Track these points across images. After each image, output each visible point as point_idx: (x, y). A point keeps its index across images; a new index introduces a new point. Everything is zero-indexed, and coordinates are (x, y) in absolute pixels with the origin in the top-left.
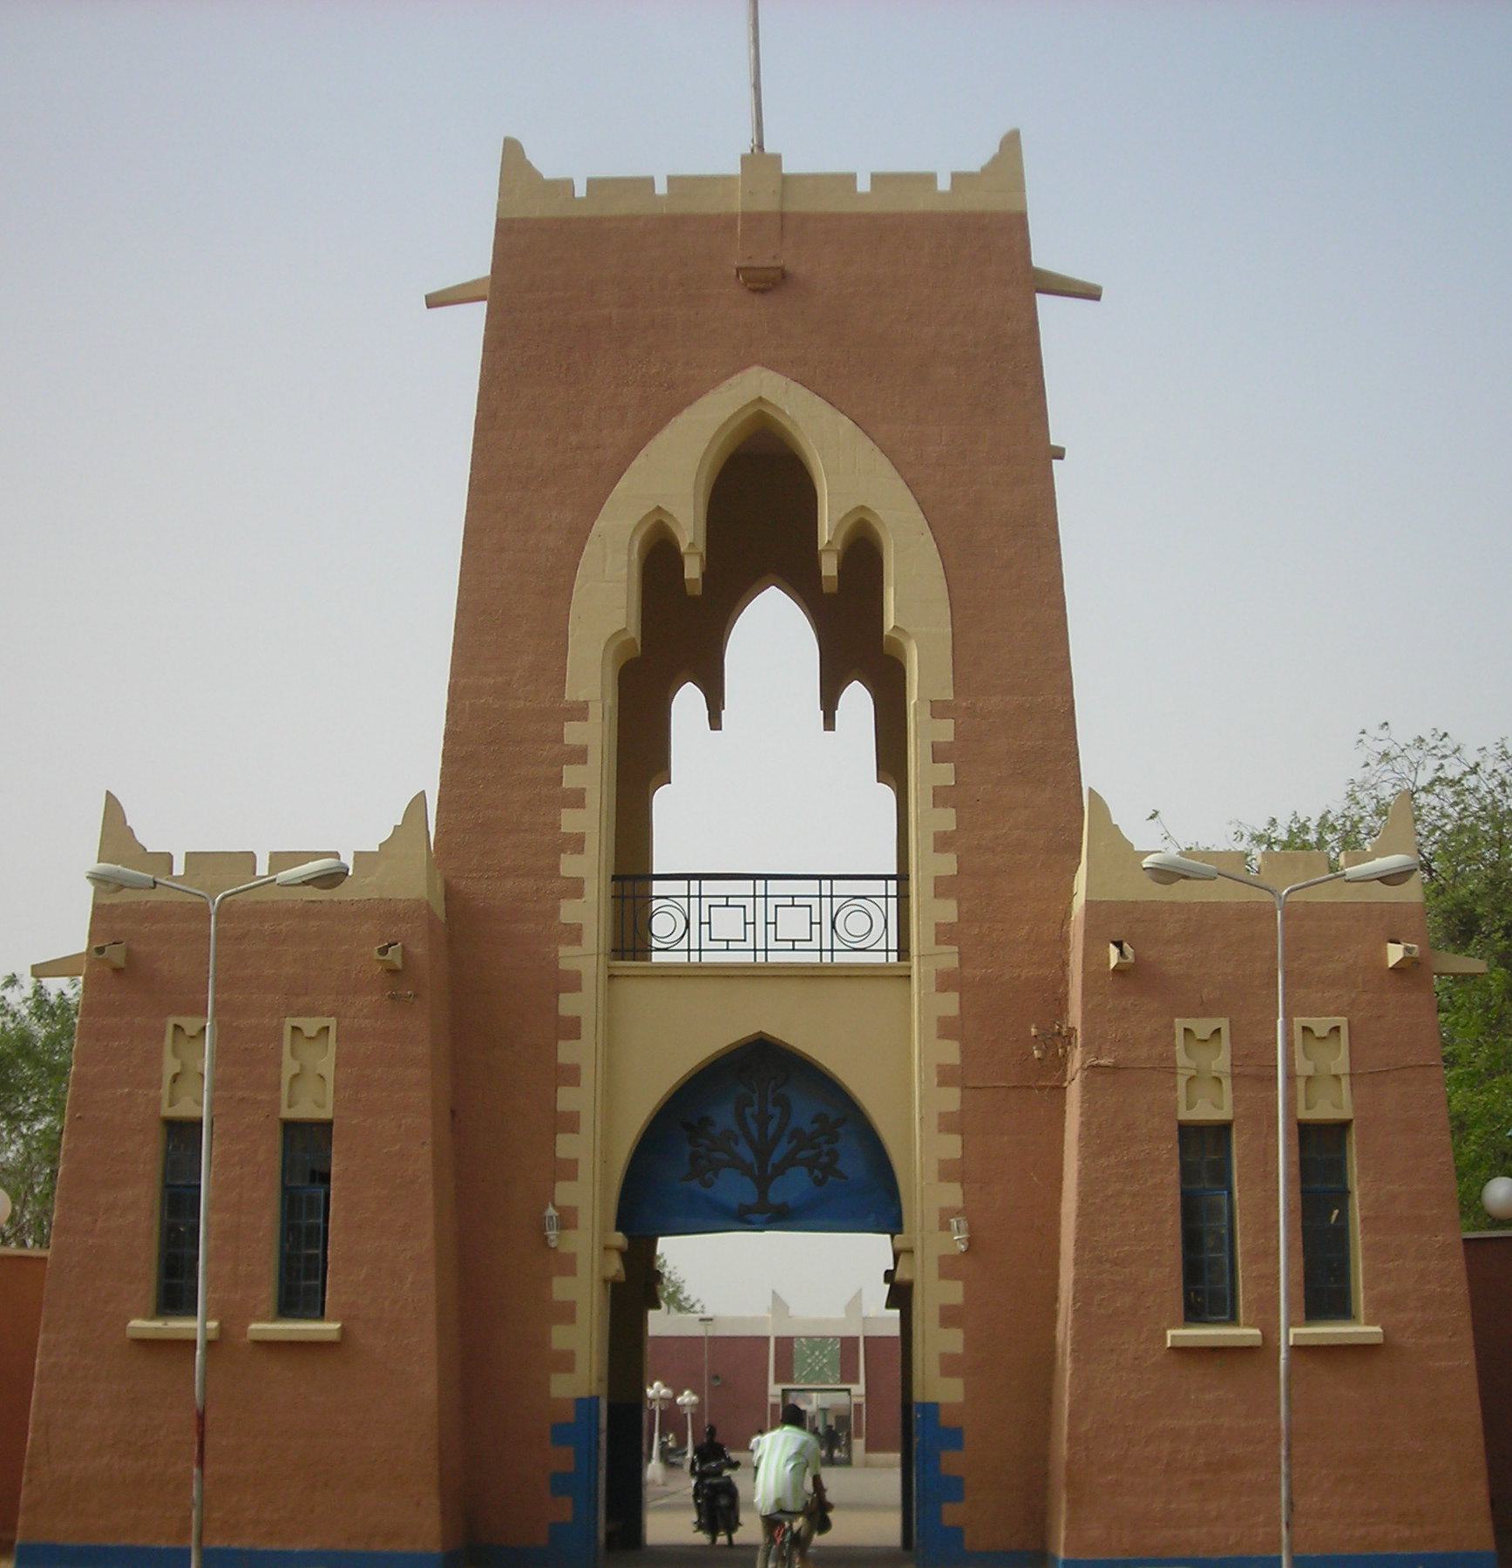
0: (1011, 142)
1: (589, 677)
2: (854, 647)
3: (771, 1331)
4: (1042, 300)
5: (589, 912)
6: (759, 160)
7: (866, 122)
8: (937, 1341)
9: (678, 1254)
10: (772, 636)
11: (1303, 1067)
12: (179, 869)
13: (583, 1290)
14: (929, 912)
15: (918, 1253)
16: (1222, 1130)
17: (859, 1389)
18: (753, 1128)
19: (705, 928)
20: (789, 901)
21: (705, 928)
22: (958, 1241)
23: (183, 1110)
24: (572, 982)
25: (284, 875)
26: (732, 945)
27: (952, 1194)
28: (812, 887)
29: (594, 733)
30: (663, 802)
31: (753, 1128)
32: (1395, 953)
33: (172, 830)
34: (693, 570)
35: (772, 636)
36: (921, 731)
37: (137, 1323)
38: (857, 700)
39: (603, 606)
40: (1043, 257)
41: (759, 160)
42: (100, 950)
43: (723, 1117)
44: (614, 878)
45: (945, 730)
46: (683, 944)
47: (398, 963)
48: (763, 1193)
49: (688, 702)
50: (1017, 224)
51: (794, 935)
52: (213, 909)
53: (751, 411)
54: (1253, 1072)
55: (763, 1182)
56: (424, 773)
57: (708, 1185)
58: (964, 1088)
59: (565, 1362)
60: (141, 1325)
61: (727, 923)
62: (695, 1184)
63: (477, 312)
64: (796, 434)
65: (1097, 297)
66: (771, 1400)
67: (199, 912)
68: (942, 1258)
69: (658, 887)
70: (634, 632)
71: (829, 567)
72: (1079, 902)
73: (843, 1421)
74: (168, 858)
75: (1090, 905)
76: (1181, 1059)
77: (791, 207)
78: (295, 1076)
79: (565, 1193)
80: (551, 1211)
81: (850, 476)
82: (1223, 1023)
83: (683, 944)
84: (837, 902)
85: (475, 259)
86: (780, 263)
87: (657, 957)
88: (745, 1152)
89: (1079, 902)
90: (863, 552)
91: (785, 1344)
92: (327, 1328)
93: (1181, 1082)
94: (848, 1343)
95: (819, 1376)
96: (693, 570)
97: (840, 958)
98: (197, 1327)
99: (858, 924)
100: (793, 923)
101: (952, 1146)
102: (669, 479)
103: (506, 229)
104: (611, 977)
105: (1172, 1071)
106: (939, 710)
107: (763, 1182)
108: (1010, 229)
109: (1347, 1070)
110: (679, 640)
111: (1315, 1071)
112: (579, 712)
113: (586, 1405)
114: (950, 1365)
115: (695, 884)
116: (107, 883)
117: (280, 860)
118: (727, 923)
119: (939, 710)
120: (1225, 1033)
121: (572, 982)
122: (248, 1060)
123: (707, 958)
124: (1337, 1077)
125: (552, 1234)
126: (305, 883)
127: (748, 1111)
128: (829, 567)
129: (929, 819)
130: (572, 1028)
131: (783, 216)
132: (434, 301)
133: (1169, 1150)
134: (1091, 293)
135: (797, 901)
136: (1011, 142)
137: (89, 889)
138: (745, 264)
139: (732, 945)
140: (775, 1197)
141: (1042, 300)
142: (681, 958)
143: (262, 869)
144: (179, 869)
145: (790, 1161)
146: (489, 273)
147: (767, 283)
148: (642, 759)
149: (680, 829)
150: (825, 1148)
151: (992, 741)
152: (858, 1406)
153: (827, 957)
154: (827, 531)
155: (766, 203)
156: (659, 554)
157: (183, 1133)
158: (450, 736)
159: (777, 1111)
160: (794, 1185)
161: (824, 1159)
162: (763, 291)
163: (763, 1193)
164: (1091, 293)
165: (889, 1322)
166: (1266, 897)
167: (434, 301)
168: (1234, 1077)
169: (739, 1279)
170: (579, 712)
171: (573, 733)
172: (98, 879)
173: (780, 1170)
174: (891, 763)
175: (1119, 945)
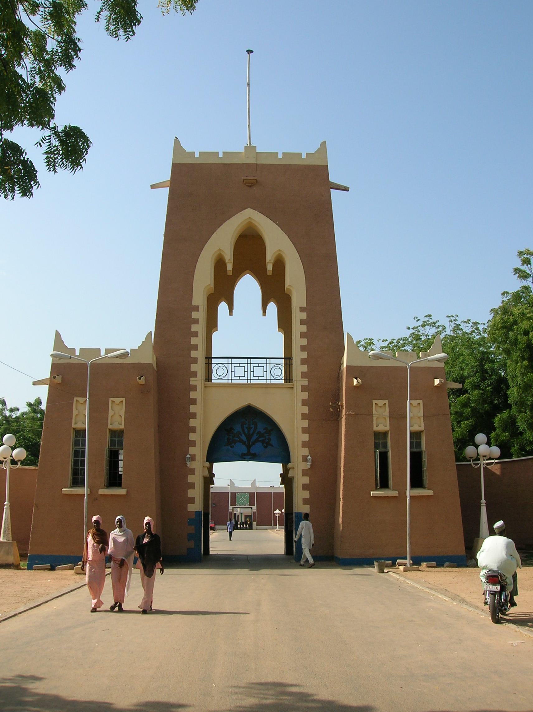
0: (324, 144)
1: (199, 298)
2: (274, 290)
3: (230, 491)
4: (332, 191)
5: (198, 368)
6: (250, 148)
7: (280, 139)
8: (300, 495)
9: (217, 467)
10: (248, 288)
11: (412, 415)
12: (77, 353)
13: (197, 479)
14: (299, 369)
15: (296, 468)
16: (385, 434)
17: (255, 508)
18: (246, 430)
19: (265, 370)
20: (257, 365)
21: (265, 370)
22: (308, 465)
23: (79, 426)
24: (194, 388)
25: (110, 355)
26: (241, 378)
27: (306, 451)
28: (245, 361)
29: (200, 315)
30: (215, 335)
31: (246, 430)
32: (437, 382)
33: (76, 342)
34: (230, 267)
35: (248, 288)
36: (297, 316)
37: (65, 490)
38: (272, 307)
39: (203, 278)
40: (333, 178)
41: (250, 148)
42: (54, 377)
43: (237, 428)
44: (206, 358)
45: (304, 316)
46: (226, 378)
47: (144, 383)
48: (249, 450)
49: (223, 307)
50: (325, 168)
51: (258, 375)
52: (89, 365)
53: (248, 221)
54: (397, 416)
55: (249, 447)
56: (150, 326)
57: (232, 447)
58: (309, 420)
59: (192, 500)
60: (65, 490)
61: (239, 371)
62: (229, 447)
63: (166, 191)
64: (259, 227)
65: (348, 191)
66: (229, 511)
67: (83, 366)
68: (303, 470)
69: (214, 361)
70: (212, 286)
71: (270, 267)
72: (345, 365)
73: (250, 517)
74: (74, 350)
75: (347, 367)
76: (374, 412)
77: (258, 163)
78: (77, 415)
79: (192, 450)
80: (188, 456)
81: (277, 241)
82: (387, 402)
83: (226, 378)
84: (272, 366)
85: (167, 176)
86: (256, 178)
87: (213, 381)
88: (244, 438)
89: (345, 365)
90: (280, 264)
91: (234, 495)
92: (122, 491)
93: (374, 418)
94: (252, 495)
95: (243, 504)
96: (230, 267)
97: (272, 382)
98: (85, 491)
99: (220, 372)
100: (259, 372)
101: (306, 437)
102: (222, 241)
103: (175, 166)
104: (205, 387)
105: (372, 415)
106: (302, 310)
107: (249, 447)
108: (324, 170)
109: (422, 415)
110: (223, 290)
111: (117, 414)
112: (196, 309)
113: (198, 514)
114: (305, 502)
115: (230, 360)
116: (56, 357)
117: (108, 351)
118: (239, 371)
119: (302, 310)
120: (422, 404)
121: (194, 388)
122: (99, 411)
123: (233, 381)
124: (419, 418)
125: (188, 463)
126: (117, 357)
127: (245, 426)
128: (270, 267)
129: (298, 342)
130: (194, 402)
131: (257, 164)
132: (153, 187)
133: (108, 434)
134: (346, 189)
135: (241, 365)
136: (324, 144)
137: (50, 359)
138: (245, 178)
139: (241, 378)
140: (252, 451)
141: (332, 191)
142: (226, 381)
143: (103, 353)
144: (77, 353)
145: (257, 441)
146: (169, 178)
147: (251, 184)
148: (212, 324)
149: (221, 344)
150: (267, 437)
151: (315, 319)
152: (254, 512)
153: (268, 382)
154: (270, 257)
155: (252, 161)
156: (220, 264)
157: (80, 433)
158: (158, 315)
159: (253, 426)
160: (257, 448)
161: (267, 441)
162: (250, 186)
163: (249, 450)
164: (346, 189)
165: (282, 489)
166: (404, 365)
167: (153, 187)
168: (389, 417)
169: (237, 475)
170: (196, 309)
171: (195, 315)
172: (52, 355)
173: (254, 443)
174: (285, 323)
175: (356, 379)
